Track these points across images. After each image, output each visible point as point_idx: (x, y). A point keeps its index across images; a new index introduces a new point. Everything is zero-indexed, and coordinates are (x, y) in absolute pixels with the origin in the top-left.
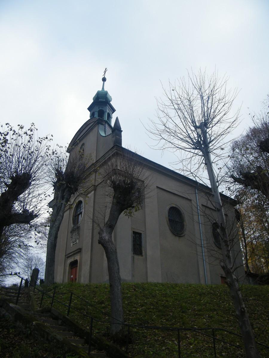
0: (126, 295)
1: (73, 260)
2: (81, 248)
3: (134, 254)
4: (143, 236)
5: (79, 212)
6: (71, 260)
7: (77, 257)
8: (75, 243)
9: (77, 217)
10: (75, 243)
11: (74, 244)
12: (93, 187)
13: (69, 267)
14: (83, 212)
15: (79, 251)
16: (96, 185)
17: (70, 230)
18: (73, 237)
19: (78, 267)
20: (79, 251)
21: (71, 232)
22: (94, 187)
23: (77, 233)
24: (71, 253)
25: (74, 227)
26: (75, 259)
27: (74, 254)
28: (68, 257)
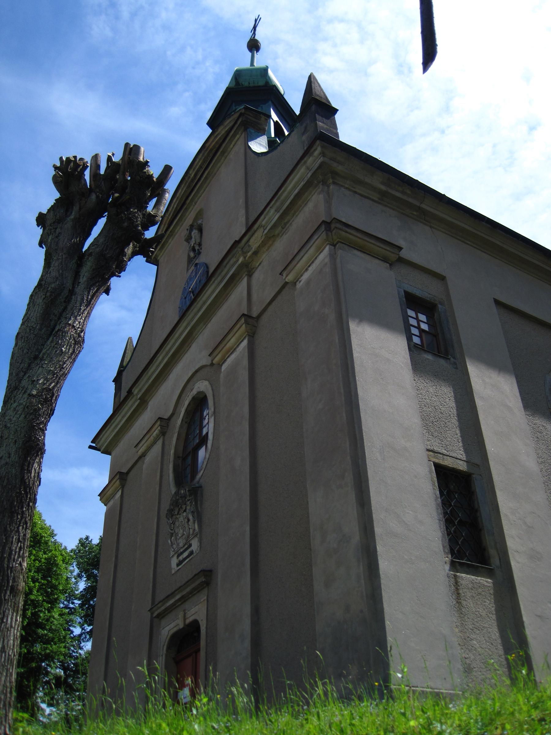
0: (296, 695)
1: (181, 626)
2: (211, 571)
3: (453, 565)
4: (478, 487)
5: (198, 437)
6: (172, 625)
7: (197, 611)
8: (185, 554)
9: (190, 458)
10: (185, 554)
11: (181, 558)
12: (243, 320)
13: (166, 655)
14: (210, 436)
15: (205, 579)
16: (255, 314)
17: (166, 506)
18: (177, 534)
19: (202, 653)
20: (205, 579)
21: (171, 514)
22: (246, 323)
23: (193, 512)
24: (172, 595)
25: (177, 493)
26: (188, 621)
27: (184, 599)
28: (161, 616)
